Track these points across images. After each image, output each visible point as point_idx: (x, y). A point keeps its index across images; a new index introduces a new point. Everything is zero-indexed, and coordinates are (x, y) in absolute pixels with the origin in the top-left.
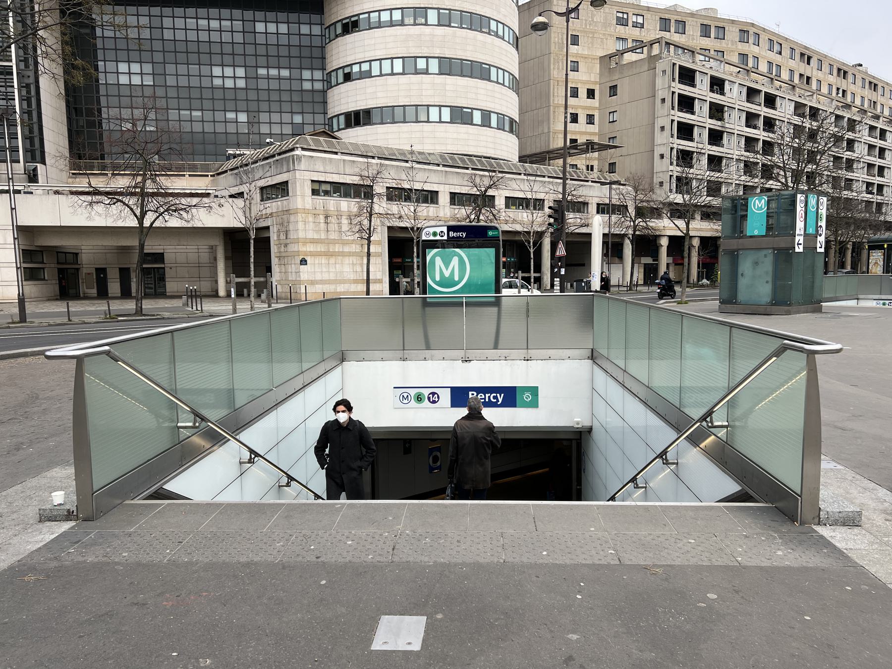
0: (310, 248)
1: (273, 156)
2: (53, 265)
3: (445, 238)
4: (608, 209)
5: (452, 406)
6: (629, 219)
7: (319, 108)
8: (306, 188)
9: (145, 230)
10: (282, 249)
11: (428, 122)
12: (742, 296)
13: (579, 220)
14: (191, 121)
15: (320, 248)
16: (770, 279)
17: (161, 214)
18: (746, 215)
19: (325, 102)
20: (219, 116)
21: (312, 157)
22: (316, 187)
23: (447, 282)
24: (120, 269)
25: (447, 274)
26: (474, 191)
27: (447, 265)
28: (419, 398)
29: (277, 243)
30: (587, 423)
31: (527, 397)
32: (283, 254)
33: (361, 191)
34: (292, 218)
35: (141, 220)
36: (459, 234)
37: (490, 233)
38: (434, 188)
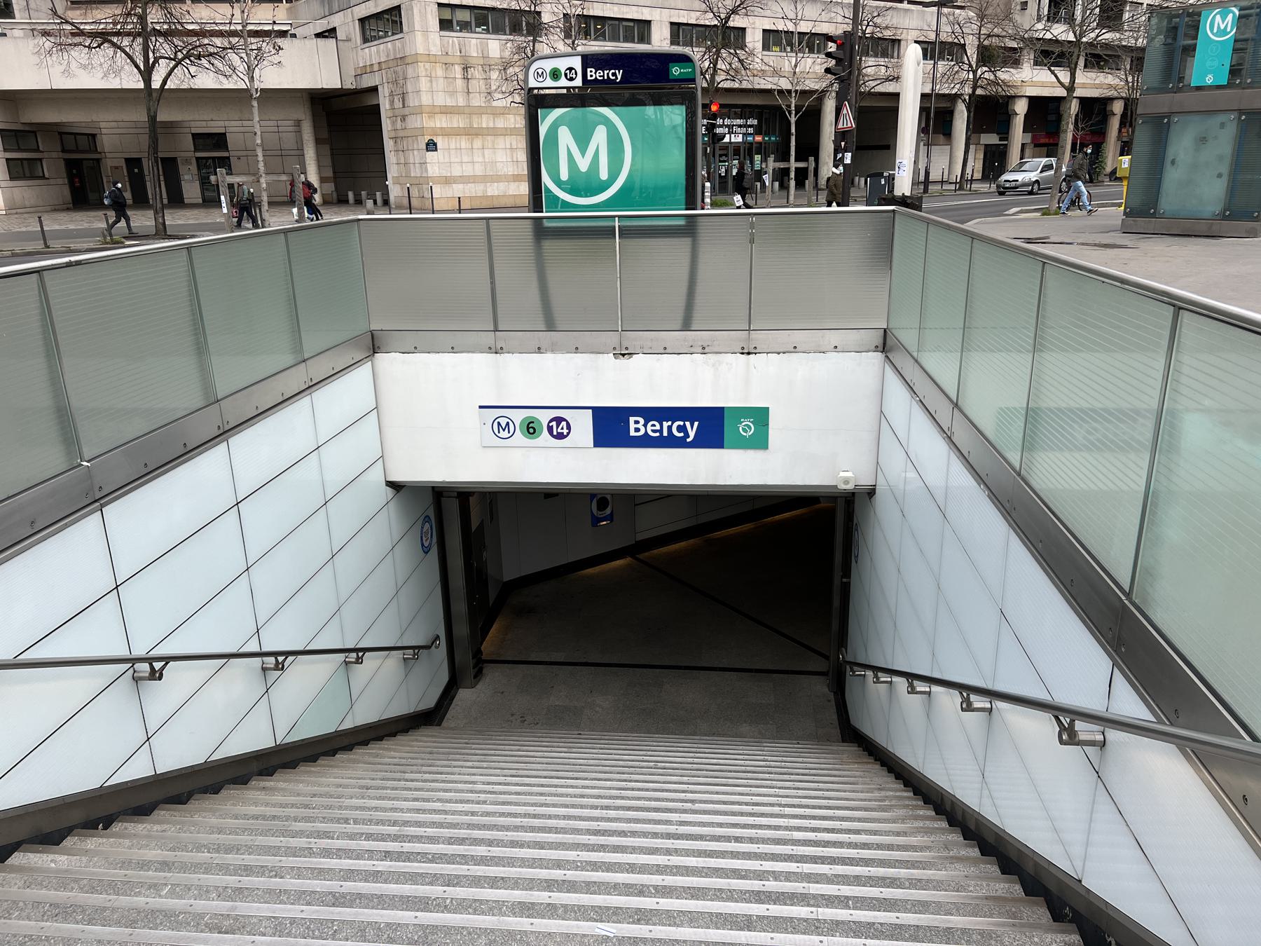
0: (441, 122)
2: (54, 155)
3: (578, 82)
4: (933, 50)
5: (595, 446)
6: (966, 67)
8: (429, 16)
9: (155, 95)
10: (399, 125)
12: (1169, 201)
13: (883, 69)
15: (458, 122)
16: (1225, 169)
17: (179, 63)
18: (1194, 48)
22: (447, 15)
23: (584, 185)
25: (583, 164)
26: (709, 20)
27: (583, 140)
28: (531, 429)
30: (866, 481)
31: (746, 428)
32: (401, 134)
34: (410, 71)
35: (147, 74)
36: (608, 74)
37: (676, 71)
38: (645, 15)
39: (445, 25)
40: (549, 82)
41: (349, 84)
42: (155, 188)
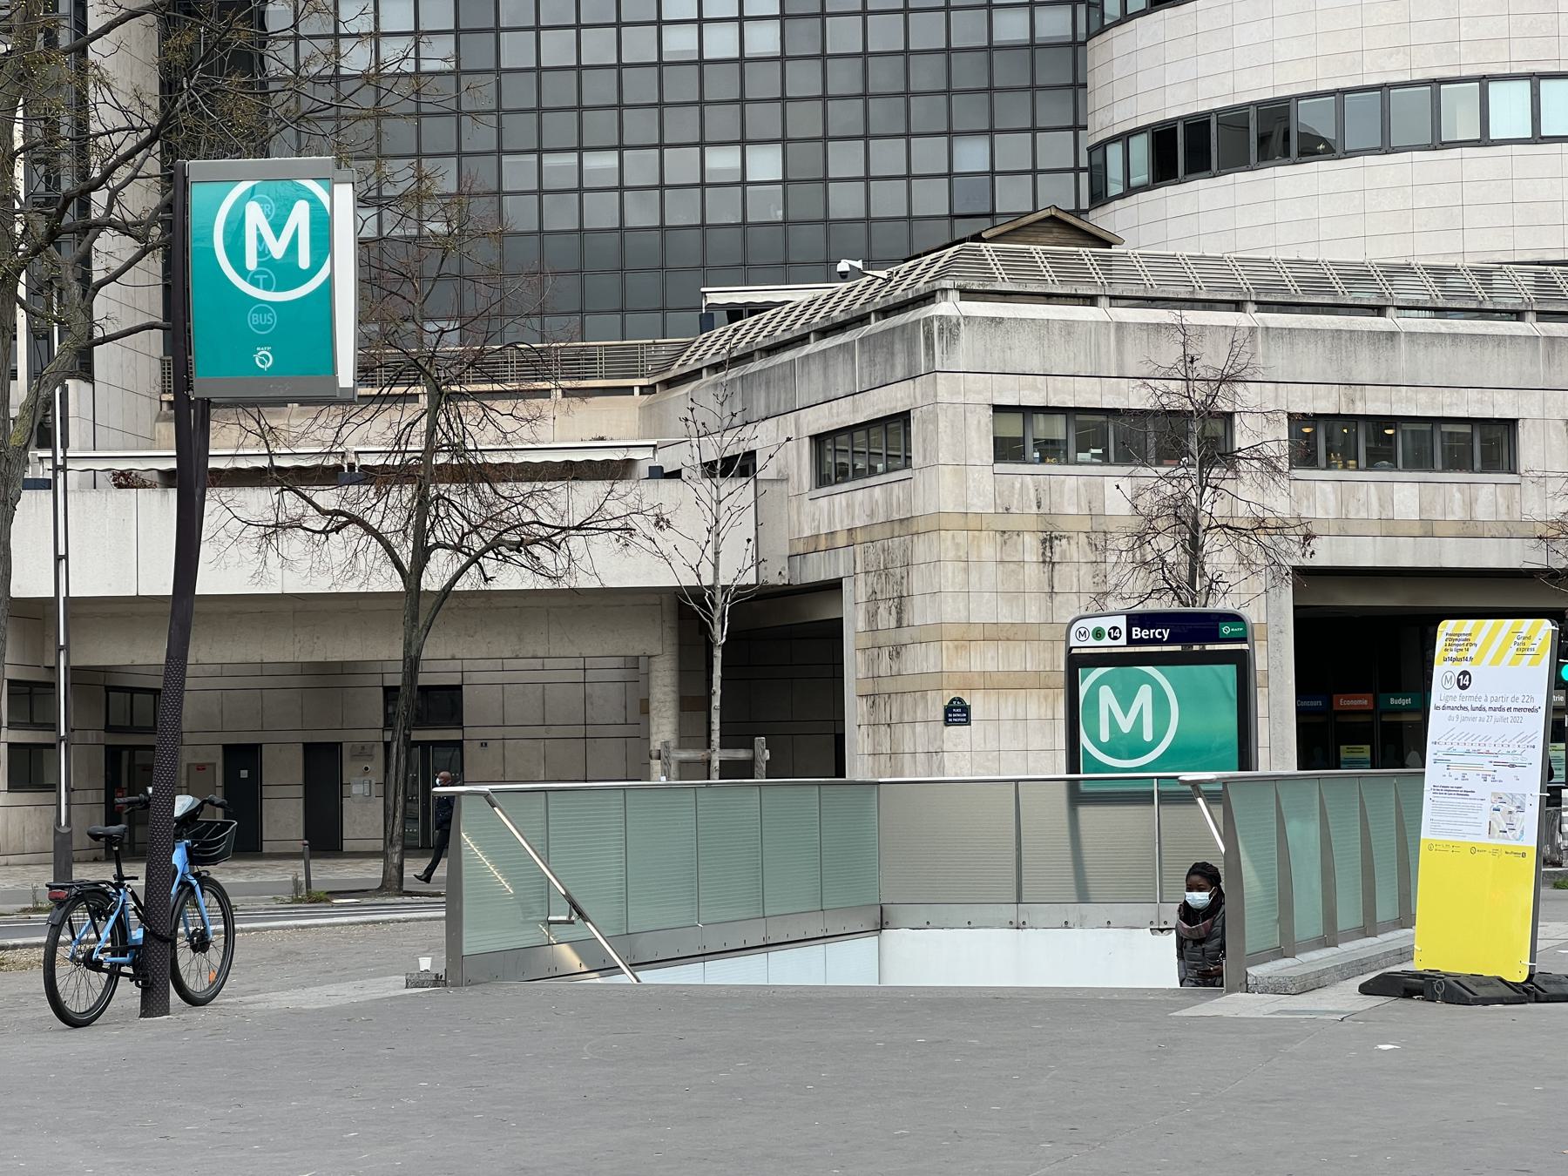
0: (983, 659)
1: (863, 319)
2: (91, 737)
3: (1123, 640)
7: (1054, 109)
8: (973, 434)
10: (884, 666)
11: (1484, 141)
14: (581, 190)
17: (474, 560)
19: (1078, 86)
20: (682, 166)
21: (997, 321)
23: (1131, 746)
24: (309, 748)
25: (1126, 725)
27: (1126, 701)
29: (865, 641)
32: (887, 685)
33: (1186, 436)
35: (412, 576)
38: (1500, 406)
39: (1006, 450)
40: (1092, 642)
41: (775, 575)
42: (284, 816)
